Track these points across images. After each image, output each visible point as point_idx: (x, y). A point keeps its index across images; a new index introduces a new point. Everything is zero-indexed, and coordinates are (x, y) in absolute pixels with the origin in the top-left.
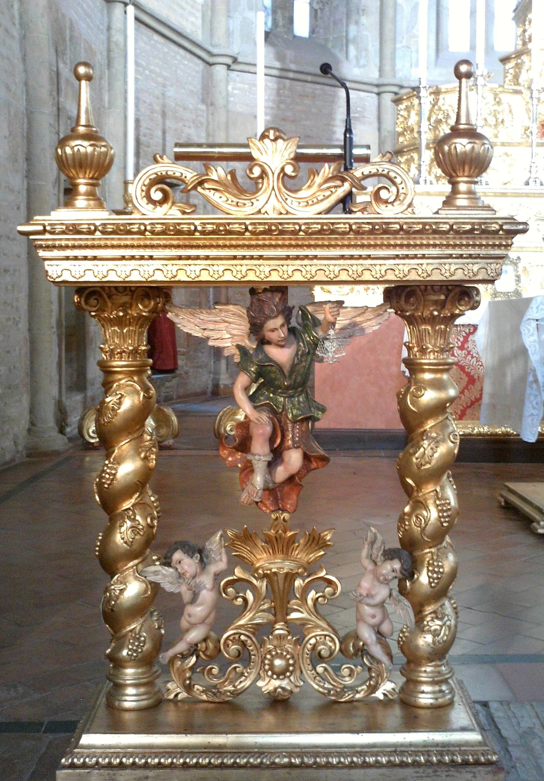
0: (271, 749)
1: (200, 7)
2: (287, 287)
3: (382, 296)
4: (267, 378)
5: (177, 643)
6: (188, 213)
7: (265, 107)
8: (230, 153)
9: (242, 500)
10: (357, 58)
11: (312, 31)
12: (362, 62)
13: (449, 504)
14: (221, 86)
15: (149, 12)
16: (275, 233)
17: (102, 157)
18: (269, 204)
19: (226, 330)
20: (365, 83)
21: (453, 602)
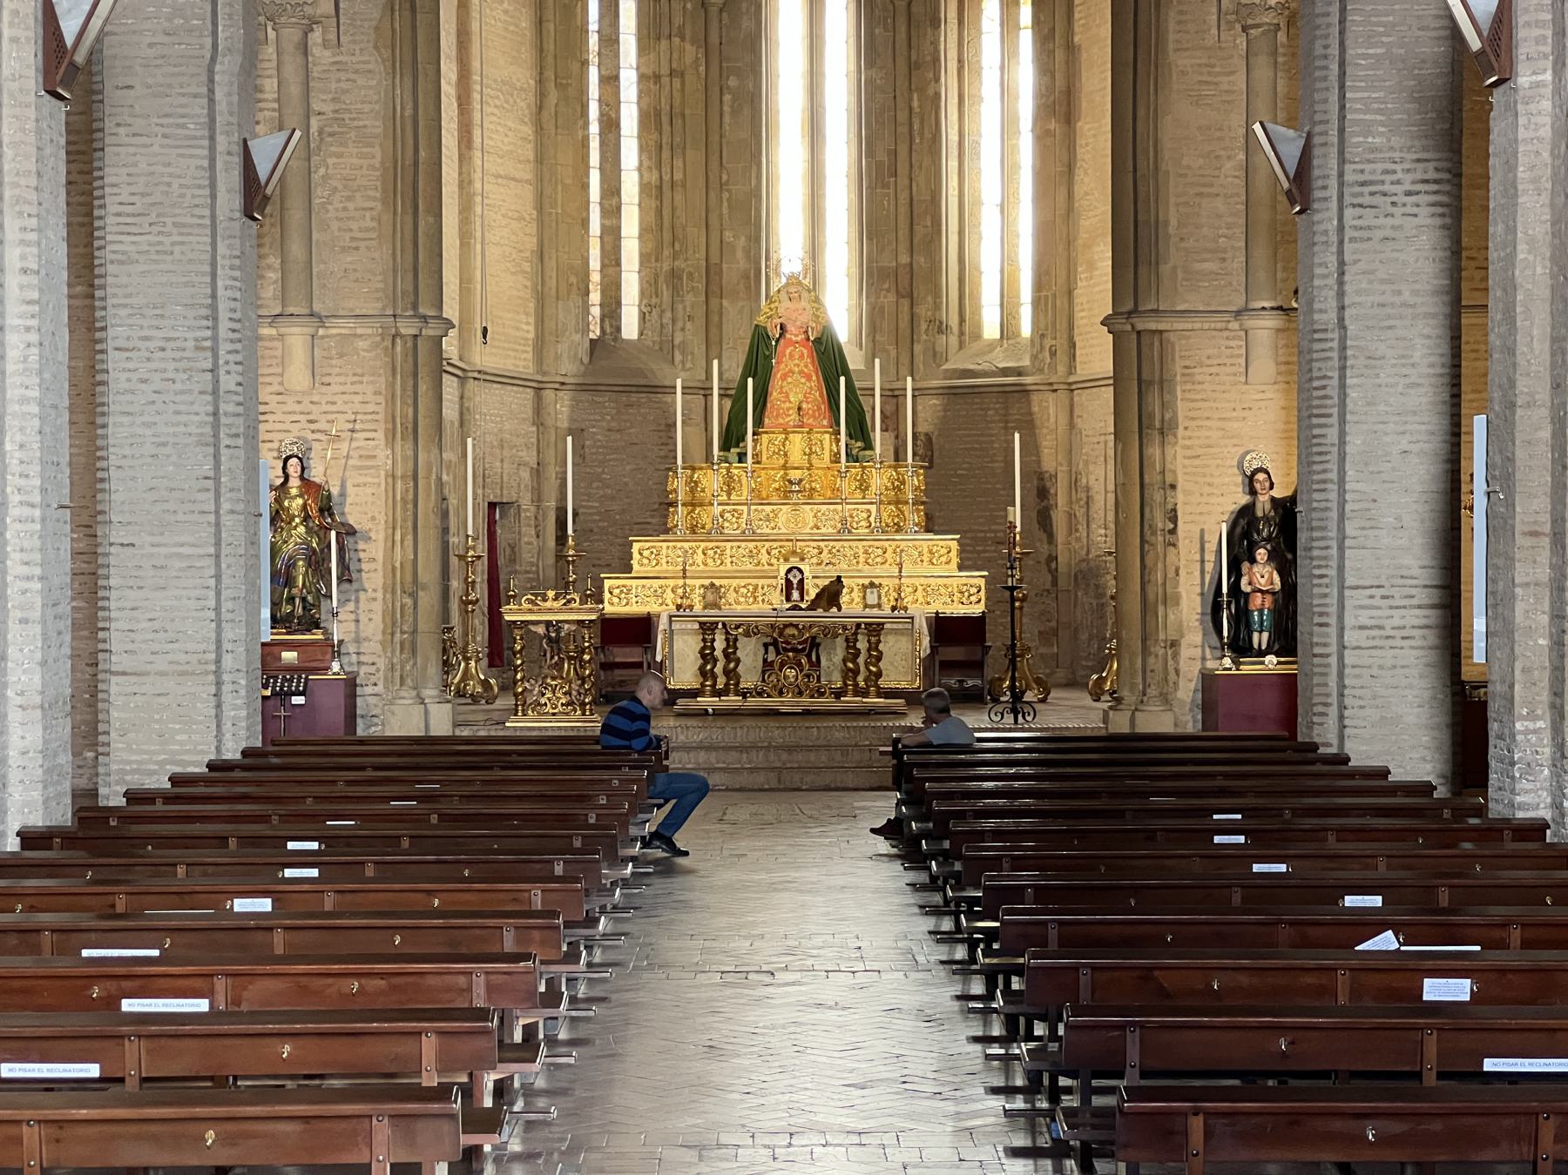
0: (393, 395)
2: (961, 568)
3: (983, 268)
4: (550, 640)
5: (1018, 313)
6: (791, 625)
7: (70, 297)
8: (288, 1103)
9: (991, 328)
10: (683, 362)
11: (641, 334)
12: (689, 365)
13: (691, 607)
14: (551, 409)
15: (1445, 348)
16: (550, 610)
17: (1440, 210)
18: (548, 604)
19: (541, 630)
20: (394, 225)
21: (750, 655)
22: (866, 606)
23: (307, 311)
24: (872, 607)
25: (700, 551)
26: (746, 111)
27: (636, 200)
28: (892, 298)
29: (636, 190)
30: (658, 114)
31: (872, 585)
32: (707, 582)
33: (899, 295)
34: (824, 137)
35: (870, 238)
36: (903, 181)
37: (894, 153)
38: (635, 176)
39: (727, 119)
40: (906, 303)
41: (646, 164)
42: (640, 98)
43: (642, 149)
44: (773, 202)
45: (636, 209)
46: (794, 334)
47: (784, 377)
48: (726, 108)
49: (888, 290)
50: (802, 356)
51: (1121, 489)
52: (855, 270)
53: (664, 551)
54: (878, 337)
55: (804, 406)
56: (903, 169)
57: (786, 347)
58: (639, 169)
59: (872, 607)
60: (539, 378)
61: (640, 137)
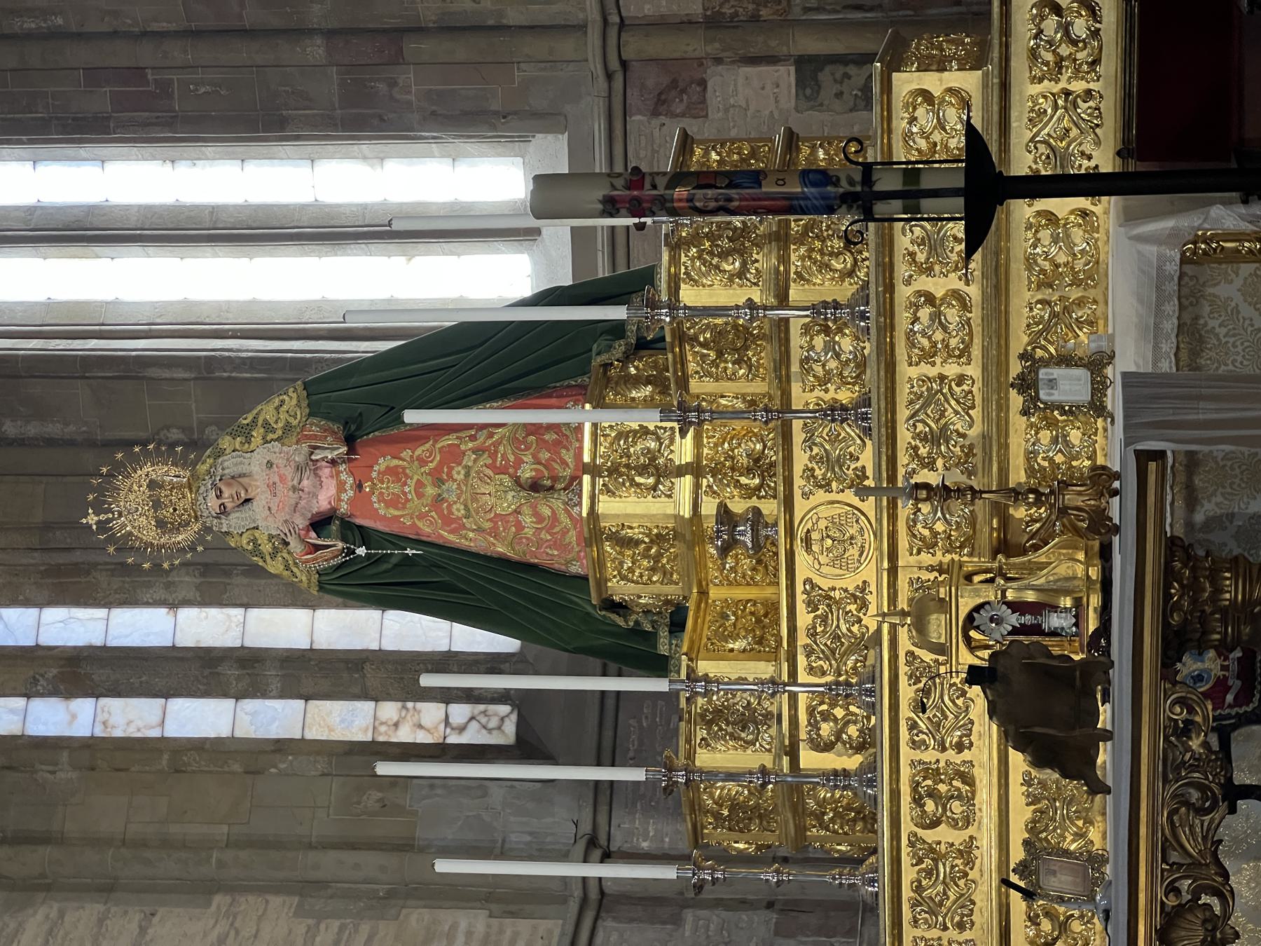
1: (495, 922)
22: (1098, 408)
23: (688, 480)
24: (1099, 387)
25: (929, 835)
26: (154, 372)
27: (237, 613)
28: (408, 76)
29: (215, 614)
30: (55, 571)
31: (1026, 384)
32: (1016, 400)
33: (397, 59)
34: (91, 209)
35: (282, 129)
36: (146, 55)
37: (94, 76)
38: (188, 615)
39: (54, 429)
40: (411, 46)
41: (161, 594)
42: (27, 603)
43: (130, 600)
44: (232, 320)
45: (254, 613)
46: (327, 493)
47: (447, 520)
48: (33, 430)
49: (393, 83)
50: (396, 474)
51: (1001, 58)
52: (365, 148)
53: (930, 756)
54: (495, 106)
55: (527, 473)
56: (122, 55)
57: (375, 514)
58: (173, 605)
59: (1099, 387)
60: (574, 906)
61: (108, 604)
